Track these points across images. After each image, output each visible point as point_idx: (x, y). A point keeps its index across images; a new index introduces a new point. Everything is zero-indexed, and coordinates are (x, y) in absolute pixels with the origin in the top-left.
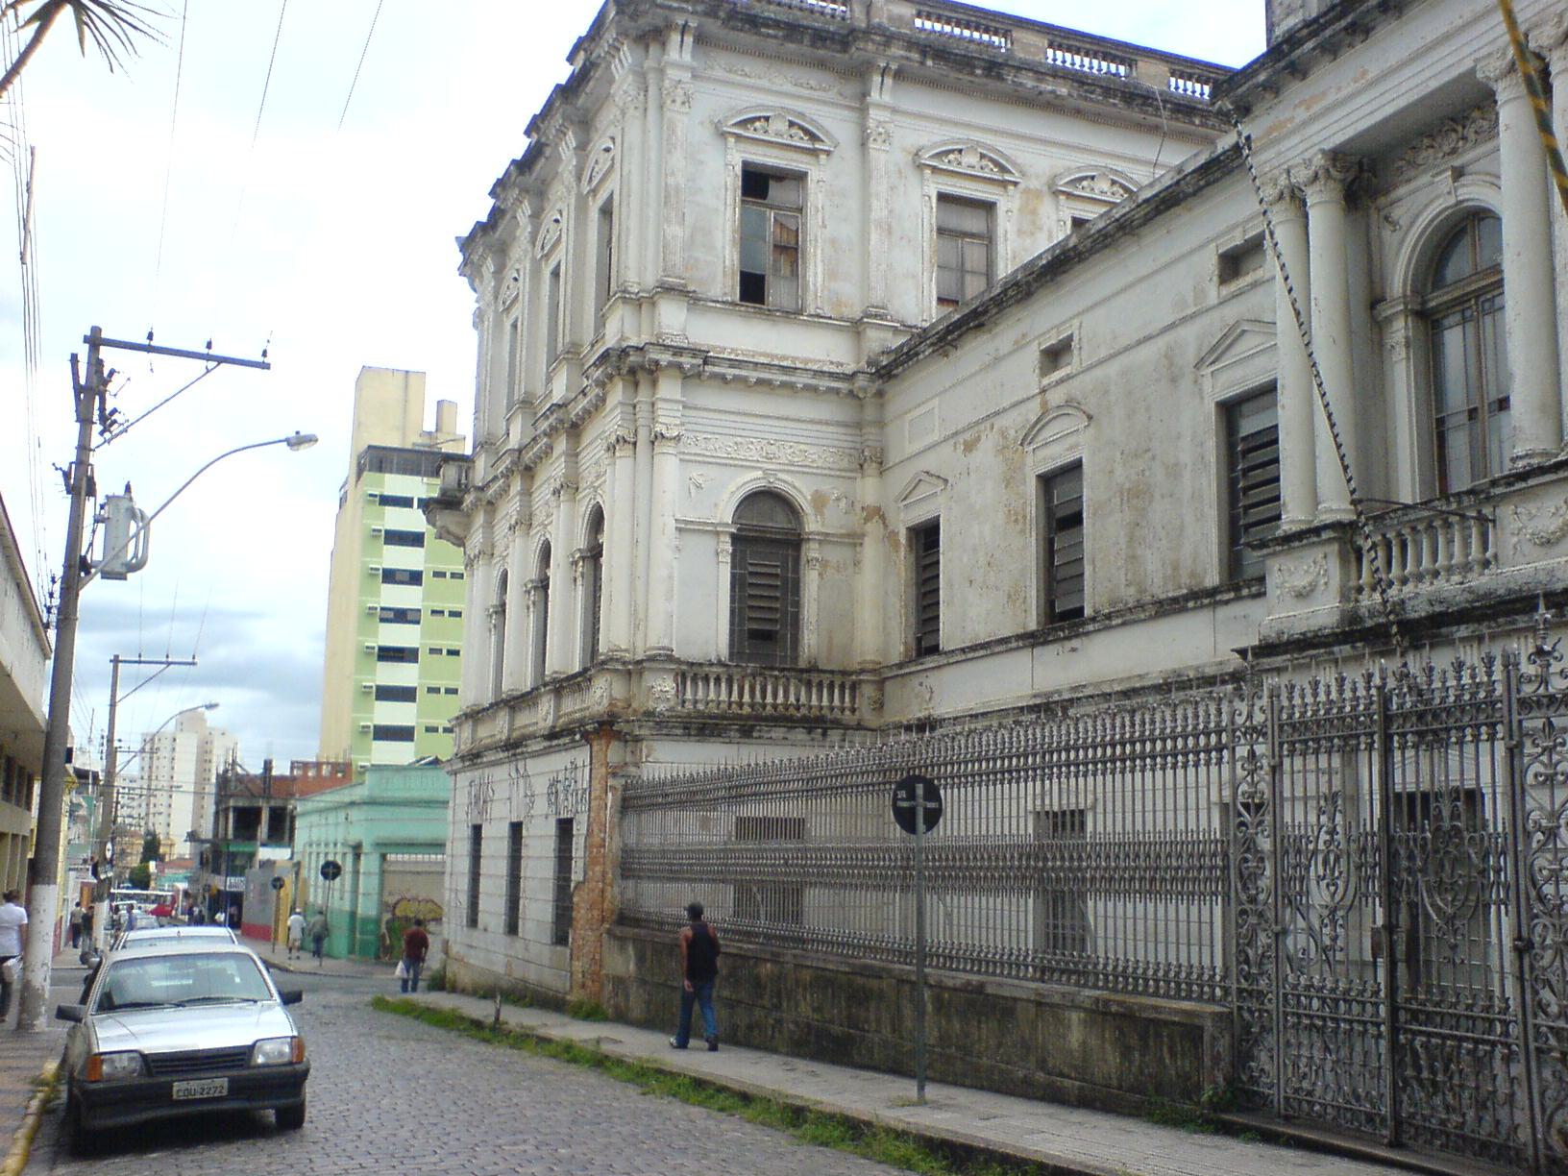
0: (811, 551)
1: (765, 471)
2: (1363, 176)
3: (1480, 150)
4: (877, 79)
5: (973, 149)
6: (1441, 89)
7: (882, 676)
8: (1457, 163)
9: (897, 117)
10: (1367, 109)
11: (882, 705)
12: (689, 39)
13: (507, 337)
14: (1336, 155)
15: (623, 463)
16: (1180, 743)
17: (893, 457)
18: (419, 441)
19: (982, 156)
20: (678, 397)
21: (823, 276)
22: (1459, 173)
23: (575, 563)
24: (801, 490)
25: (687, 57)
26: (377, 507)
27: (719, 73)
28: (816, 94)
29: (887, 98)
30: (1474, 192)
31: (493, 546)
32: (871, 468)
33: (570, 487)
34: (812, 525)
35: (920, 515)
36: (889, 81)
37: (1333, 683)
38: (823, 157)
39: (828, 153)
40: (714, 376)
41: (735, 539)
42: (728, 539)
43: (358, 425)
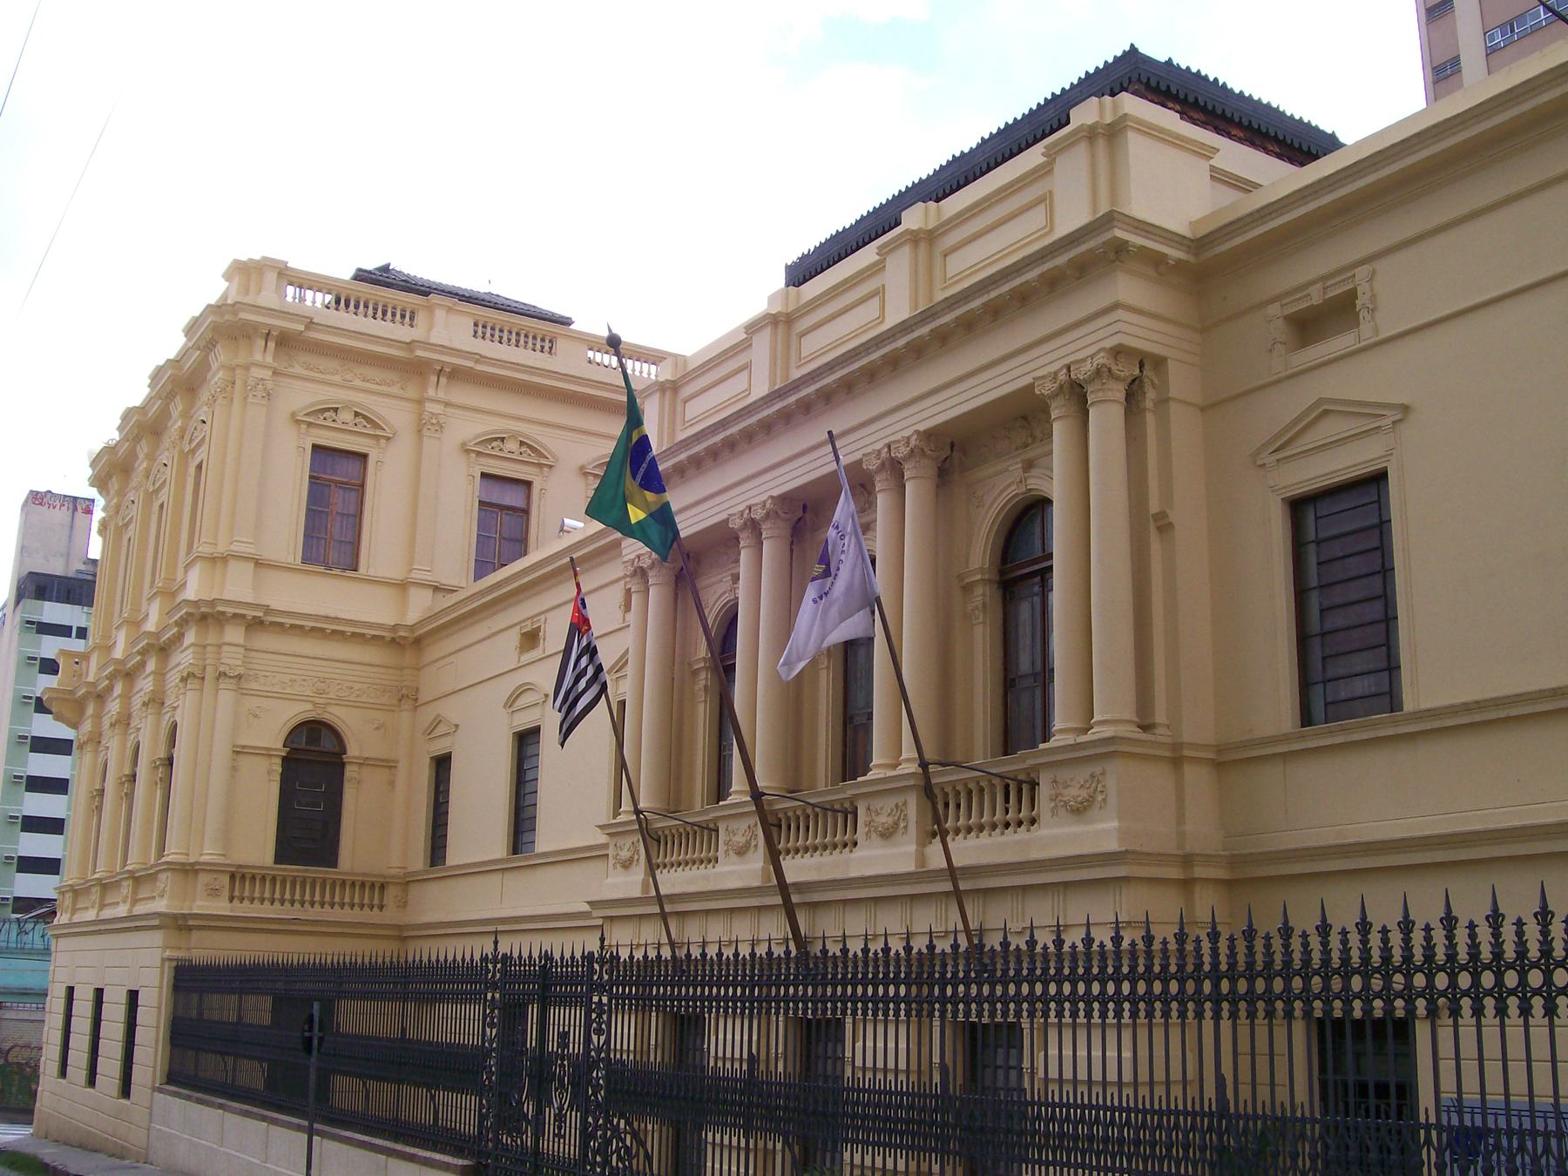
0: (350, 772)
1: (314, 704)
2: (953, 453)
3: (1039, 451)
4: (434, 379)
5: (513, 437)
6: (947, 422)
7: (408, 882)
8: (1030, 454)
9: (450, 410)
10: (805, 469)
11: (406, 903)
12: (272, 345)
13: (155, 518)
14: (784, 499)
15: (190, 698)
16: (1012, 989)
17: (423, 698)
18: (82, 567)
19: (522, 443)
20: (241, 641)
21: (382, 545)
22: (1029, 466)
23: (156, 768)
24: (345, 719)
25: (269, 359)
26: (34, 636)
27: (298, 370)
28: (384, 389)
29: (441, 395)
30: (1036, 484)
31: (129, 716)
32: (407, 705)
33: (157, 701)
34: (353, 751)
35: (439, 748)
36: (443, 380)
37: (1204, 937)
38: (383, 441)
39: (388, 439)
40: (272, 623)
41: (284, 759)
42: (279, 761)
43: (24, 550)
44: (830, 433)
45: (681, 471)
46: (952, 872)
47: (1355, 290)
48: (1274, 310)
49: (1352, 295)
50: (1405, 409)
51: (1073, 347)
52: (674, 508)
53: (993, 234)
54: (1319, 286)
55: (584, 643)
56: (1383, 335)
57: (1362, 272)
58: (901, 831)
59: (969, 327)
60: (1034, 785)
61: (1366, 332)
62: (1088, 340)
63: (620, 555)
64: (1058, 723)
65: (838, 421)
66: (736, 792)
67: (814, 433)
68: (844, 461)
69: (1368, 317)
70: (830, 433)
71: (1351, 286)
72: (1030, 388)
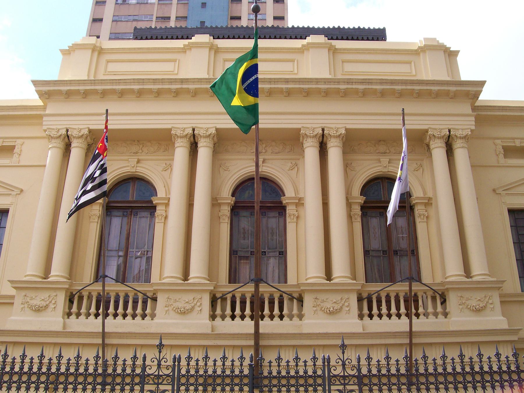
6: (152, 129)
10: (368, 122)
44: (107, 110)
45: (271, 93)
46: (104, 334)
47: (15, 146)
48: (498, 142)
49: (13, 147)
50: (22, 191)
51: (436, 122)
52: (260, 110)
53: (128, 64)
54: (519, 140)
55: (102, 163)
56: (21, 164)
57: (19, 141)
58: (49, 310)
59: (345, 94)
60: (155, 299)
61: (14, 160)
62: (212, 121)
63: (41, 124)
64: (53, 273)
65: (114, 107)
66: (52, 276)
67: (100, 107)
68: (407, 127)
69: (17, 156)
70: (107, 110)
71: (14, 144)
72: (170, 130)
